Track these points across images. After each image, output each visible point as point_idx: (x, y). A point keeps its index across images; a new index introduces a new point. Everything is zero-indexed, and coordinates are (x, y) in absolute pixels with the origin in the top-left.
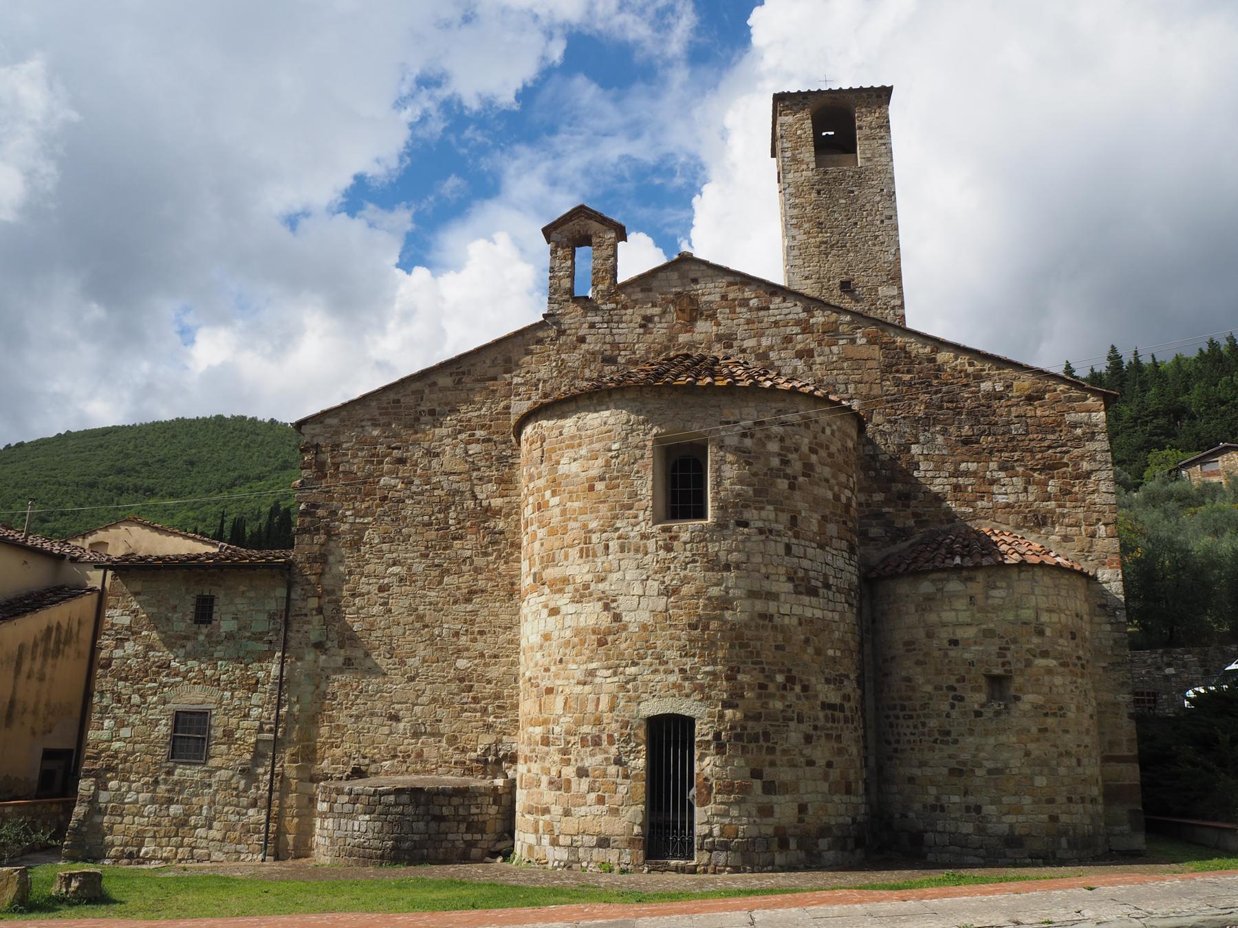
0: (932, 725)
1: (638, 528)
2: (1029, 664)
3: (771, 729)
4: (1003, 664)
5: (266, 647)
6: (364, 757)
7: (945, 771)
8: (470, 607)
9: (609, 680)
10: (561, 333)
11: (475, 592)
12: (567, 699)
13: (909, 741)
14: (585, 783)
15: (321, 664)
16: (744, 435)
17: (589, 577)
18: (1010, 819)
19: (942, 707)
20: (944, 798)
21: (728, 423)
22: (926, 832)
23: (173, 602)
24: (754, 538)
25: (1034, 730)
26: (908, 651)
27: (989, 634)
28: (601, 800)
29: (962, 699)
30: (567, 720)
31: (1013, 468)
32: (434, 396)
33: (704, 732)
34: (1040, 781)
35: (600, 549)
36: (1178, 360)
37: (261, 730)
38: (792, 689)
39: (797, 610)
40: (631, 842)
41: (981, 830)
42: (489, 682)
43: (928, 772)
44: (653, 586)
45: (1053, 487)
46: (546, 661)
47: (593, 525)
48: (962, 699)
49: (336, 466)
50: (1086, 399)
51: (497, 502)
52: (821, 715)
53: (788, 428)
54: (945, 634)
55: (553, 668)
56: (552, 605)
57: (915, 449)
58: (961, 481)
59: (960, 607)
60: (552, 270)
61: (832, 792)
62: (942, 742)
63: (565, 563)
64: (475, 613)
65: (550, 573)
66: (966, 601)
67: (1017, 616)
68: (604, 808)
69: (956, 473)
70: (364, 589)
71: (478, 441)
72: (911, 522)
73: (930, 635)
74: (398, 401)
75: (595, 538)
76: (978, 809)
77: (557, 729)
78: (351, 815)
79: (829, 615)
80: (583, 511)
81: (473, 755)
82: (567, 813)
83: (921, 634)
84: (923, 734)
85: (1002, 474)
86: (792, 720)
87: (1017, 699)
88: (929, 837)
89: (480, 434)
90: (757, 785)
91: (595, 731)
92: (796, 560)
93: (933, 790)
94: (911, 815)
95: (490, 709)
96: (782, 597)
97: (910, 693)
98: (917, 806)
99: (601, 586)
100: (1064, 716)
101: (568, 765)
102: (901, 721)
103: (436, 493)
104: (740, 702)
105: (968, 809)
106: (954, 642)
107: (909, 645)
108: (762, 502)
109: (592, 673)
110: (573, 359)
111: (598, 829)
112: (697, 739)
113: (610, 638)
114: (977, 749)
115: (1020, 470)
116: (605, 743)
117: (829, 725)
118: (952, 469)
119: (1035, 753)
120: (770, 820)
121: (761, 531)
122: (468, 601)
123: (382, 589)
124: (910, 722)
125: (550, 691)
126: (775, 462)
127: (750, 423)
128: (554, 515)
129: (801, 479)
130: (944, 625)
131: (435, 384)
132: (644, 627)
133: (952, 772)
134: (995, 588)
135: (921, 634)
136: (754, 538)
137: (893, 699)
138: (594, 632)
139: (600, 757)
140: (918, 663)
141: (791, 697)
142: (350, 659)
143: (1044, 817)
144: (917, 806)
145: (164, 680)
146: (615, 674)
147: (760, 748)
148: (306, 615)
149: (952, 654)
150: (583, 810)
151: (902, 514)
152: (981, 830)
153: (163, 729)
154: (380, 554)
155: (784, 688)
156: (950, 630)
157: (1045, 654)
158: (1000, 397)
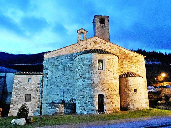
8: (68, 80)
10: (80, 45)
14: (90, 103)
17: (89, 77)
27: (134, 84)
28: (92, 105)
30: (87, 95)
35: (91, 73)
36: (148, 52)
41: (134, 107)
47: (90, 70)
51: (71, 67)
55: (84, 89)
58: (128, 66)
65: (83, 76)
69: (128, 65)
76: (133, 105)
82: (87, 107)
85: (133, 66)
89: (69, 57)
107: (125, 85)
110: (81, 48)
123: (56, 78)
125: (84, 91)
126: (112, 63)
128: (84, 69)
139: (92, 100)
141: (114, 92)
145: (24, 90)
150: (90, 107)
153: (24, 97)
158: (133, 56)
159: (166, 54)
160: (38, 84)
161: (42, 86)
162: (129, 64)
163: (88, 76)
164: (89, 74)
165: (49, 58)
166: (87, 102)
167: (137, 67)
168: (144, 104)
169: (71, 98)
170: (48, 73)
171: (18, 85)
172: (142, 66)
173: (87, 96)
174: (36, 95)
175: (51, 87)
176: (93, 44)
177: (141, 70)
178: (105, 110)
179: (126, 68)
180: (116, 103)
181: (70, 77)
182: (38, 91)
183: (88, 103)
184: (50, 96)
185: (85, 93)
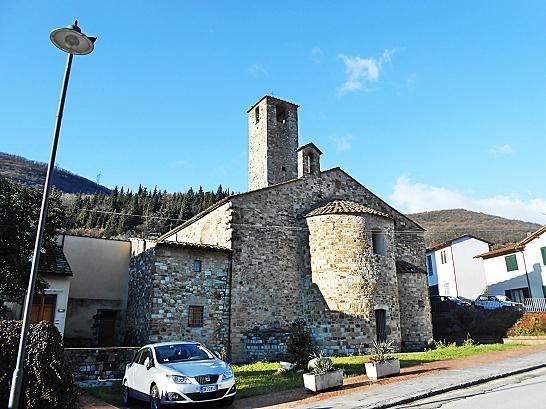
14: (359, 330)
28: (365, 334)
65: (339, 265)
110: (310, 194)
125: (342, 302)
160: (220, 278)
161: (230, 283)
166: (353, 326)
169: (295, 317)
171: (167, 279)
174: (217, 309)
176: (332, 187)
178: (209, 389)
182: (219, 297)
184: (249, 313)
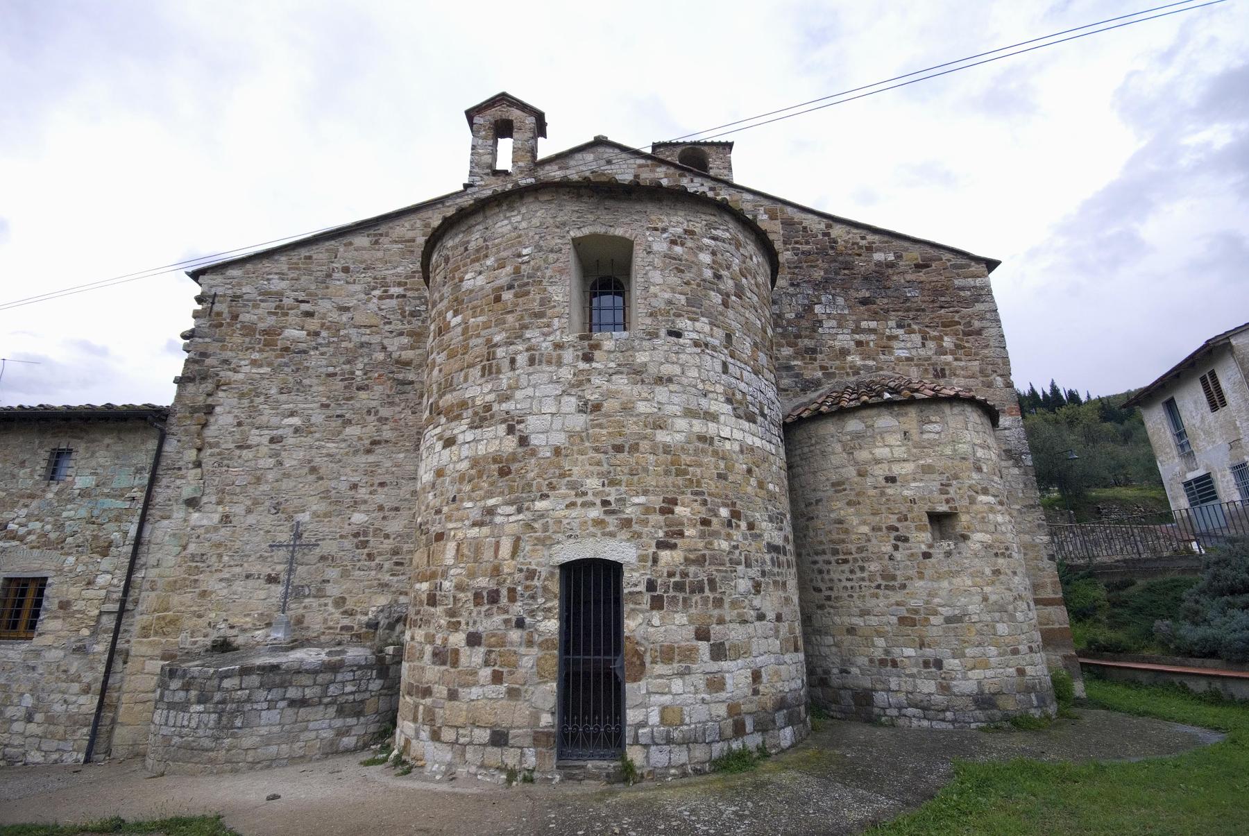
0: (872, 568)
1: (551, 338)
2: (972, 501)
3: (718, 577)
4: (947, 501)
5: (127, 505)
6: (232, 627)
7: (894, 620)
9: (512, 519)
11: (379, 443)
12: (459, 545)
13: (845, 588)
14: (478, 654)
15: (192, 523)
16: (673, 242)
18: (976, 674)
19: (883, 549)
20: (896, 651)
21: (656, 229)
22: (876, 691)
23: (22, 457)
24: (689, 350)
25: (988, 571)
26: (836, 491)
27: (928, 469)
28: (497, 678)
29: (906, 540)
31: (909, 325)
32: (349, 255)
33: (634, 580)
34: (1002, 628)
35: (506, 364)
37: (106, 599)
38: (738, 526)
39: (738, 435)
40: (539, 738)
41: (945, 689)
42: (387, 536)
43: (873, 621)
44: (570, 403)
45: (948, 342)
46: (437, 502)
48: (906, 540)
49: (235, 317)
50: (970, 266)
51: (408, 355)
52: (767, 557)
53: (719, 244)
54: (880, 471)
55: (445, 509)
56: (448, 434)
57: (818, 309)
59: (893, 442)
60: (474, 147)
61: (784, 651)
62: (887, 587)
63: (465, 386)
64: (377, 464)
65: (449, 399)
66: (899, 436)
67: (955, 450)
68: (503, 688)
70: (253, 440)
71: (391, 297)
72: (820, 374)
73: (862, 474)
74: (310, 258)
75: (500, 352)
76: (939, 664)
77: (447, 584)
78: (183, 706)
79: (768, 447)
80: (486, 326)
81: (365, 619)
82: (453, 695)
83: (851, 472)
84: (863, 579)
85: (901, 331)
86: (739, 563)
87: (965, 538)
88: (880, 697)
89: (395, 290)
90: (704, 646)
91: (493, 586)
92: (734, 381)
93: (880, 642)
94: (854, 670)
95: (387, 565)
96: (722, 418)
97: (842, 536)
98: (862, 660)
99: (504, 406)
100: (1010, 556)
101: (457, 630)
102: (833, 567)
103: (344, 345)
104: (679, 541)
105: (926, 664)
106: (891, 480)
108: (694, 313)
109: (491, 511)
111: (493, 720)
112: (626, 591)
113: (514, 467)
114: (929, 595)
115: (915, 327)
116: (504, 601)
117: (776, 570)
118: (853, 326)
119: (993, 598)
120: (723, 695)
121: (696, 344)
122: (369, 452)
124: (846, 567)
125: (440, 537)
126: (708, 274)
127: (679, 230)
128: (455, 337)
129: (733, 298)
130: (878, 462)
131: (351, 244)
132: (557, 451)
133: (902, 620)
134: (931, 422)
135: (851, 472)
136: (689, 350)
137: (821, 543)
138: (495, 461)
139: (498, 619)
140: (849, 504)
141: (737, 535)
142: (227, 517)
143: (1012, 671)
144: (862, 660)
146: (519, 511)
147: (706, 600)
148: (180, 469)
149: (890, 491)
150: (475, 692)
151: (810, 366)
152: (945, 689)
154: (276, 405)
155: (729, 524)
156: (885, 466)
157: (985, 491)
158: (891, 265)
159: (1053, 387)
162: (864, 324)
163: (478, 391)
164: (490, 371)
165: (235, 298)
166: (458, 639)
167: (931, 345)
168: (319, 618)
169: (382, 600)
170: (210, 410)
172: (979, 332)
173: (460, 587)
175: (226, 519)
177: (975, 365)
179: (844, 352)
180: (757, 646)
181: (387, 434)
183: (465, 651)
184: (204, 594)
185: (449, 556)
